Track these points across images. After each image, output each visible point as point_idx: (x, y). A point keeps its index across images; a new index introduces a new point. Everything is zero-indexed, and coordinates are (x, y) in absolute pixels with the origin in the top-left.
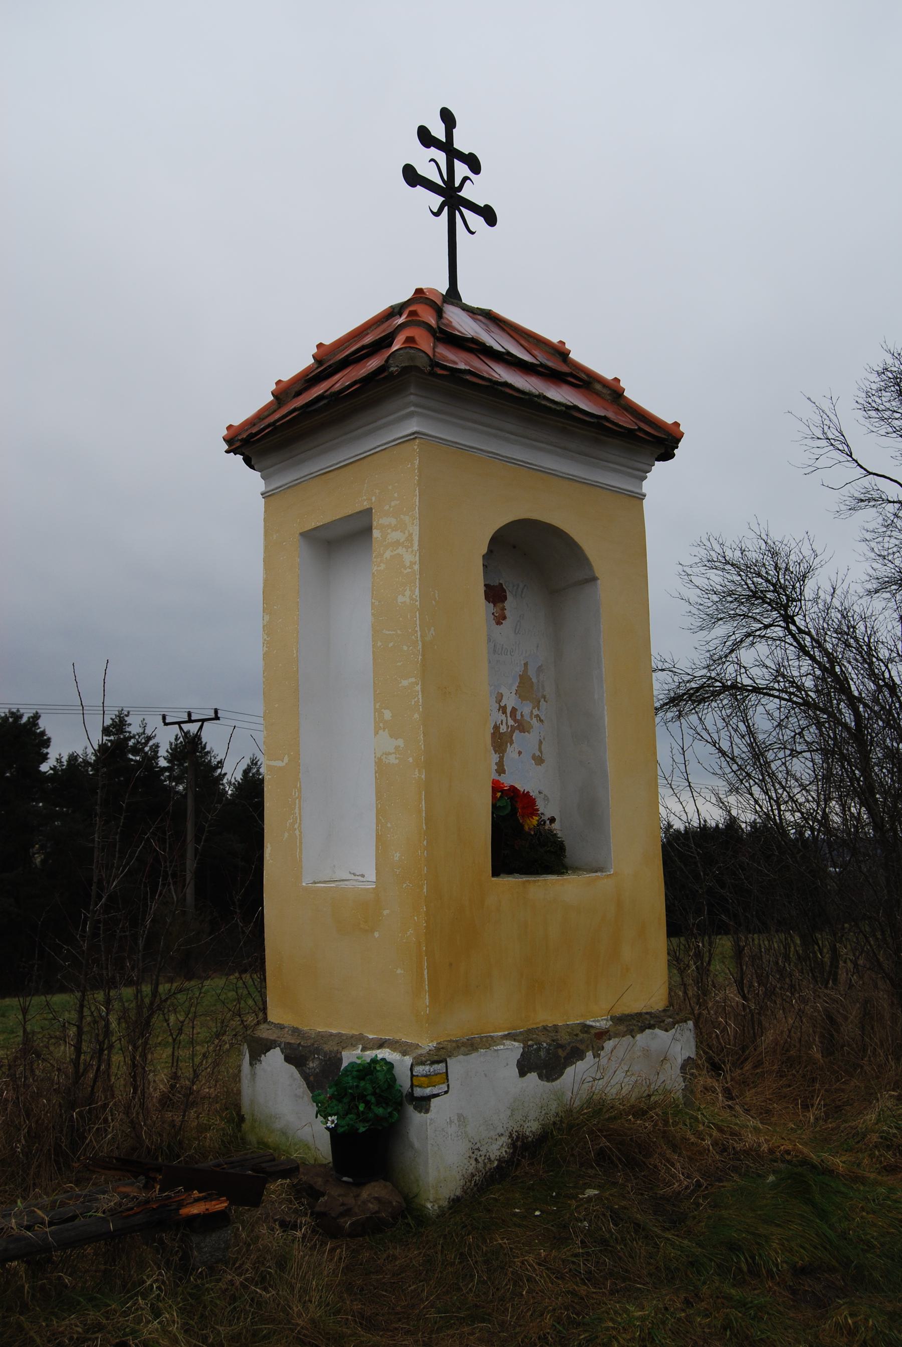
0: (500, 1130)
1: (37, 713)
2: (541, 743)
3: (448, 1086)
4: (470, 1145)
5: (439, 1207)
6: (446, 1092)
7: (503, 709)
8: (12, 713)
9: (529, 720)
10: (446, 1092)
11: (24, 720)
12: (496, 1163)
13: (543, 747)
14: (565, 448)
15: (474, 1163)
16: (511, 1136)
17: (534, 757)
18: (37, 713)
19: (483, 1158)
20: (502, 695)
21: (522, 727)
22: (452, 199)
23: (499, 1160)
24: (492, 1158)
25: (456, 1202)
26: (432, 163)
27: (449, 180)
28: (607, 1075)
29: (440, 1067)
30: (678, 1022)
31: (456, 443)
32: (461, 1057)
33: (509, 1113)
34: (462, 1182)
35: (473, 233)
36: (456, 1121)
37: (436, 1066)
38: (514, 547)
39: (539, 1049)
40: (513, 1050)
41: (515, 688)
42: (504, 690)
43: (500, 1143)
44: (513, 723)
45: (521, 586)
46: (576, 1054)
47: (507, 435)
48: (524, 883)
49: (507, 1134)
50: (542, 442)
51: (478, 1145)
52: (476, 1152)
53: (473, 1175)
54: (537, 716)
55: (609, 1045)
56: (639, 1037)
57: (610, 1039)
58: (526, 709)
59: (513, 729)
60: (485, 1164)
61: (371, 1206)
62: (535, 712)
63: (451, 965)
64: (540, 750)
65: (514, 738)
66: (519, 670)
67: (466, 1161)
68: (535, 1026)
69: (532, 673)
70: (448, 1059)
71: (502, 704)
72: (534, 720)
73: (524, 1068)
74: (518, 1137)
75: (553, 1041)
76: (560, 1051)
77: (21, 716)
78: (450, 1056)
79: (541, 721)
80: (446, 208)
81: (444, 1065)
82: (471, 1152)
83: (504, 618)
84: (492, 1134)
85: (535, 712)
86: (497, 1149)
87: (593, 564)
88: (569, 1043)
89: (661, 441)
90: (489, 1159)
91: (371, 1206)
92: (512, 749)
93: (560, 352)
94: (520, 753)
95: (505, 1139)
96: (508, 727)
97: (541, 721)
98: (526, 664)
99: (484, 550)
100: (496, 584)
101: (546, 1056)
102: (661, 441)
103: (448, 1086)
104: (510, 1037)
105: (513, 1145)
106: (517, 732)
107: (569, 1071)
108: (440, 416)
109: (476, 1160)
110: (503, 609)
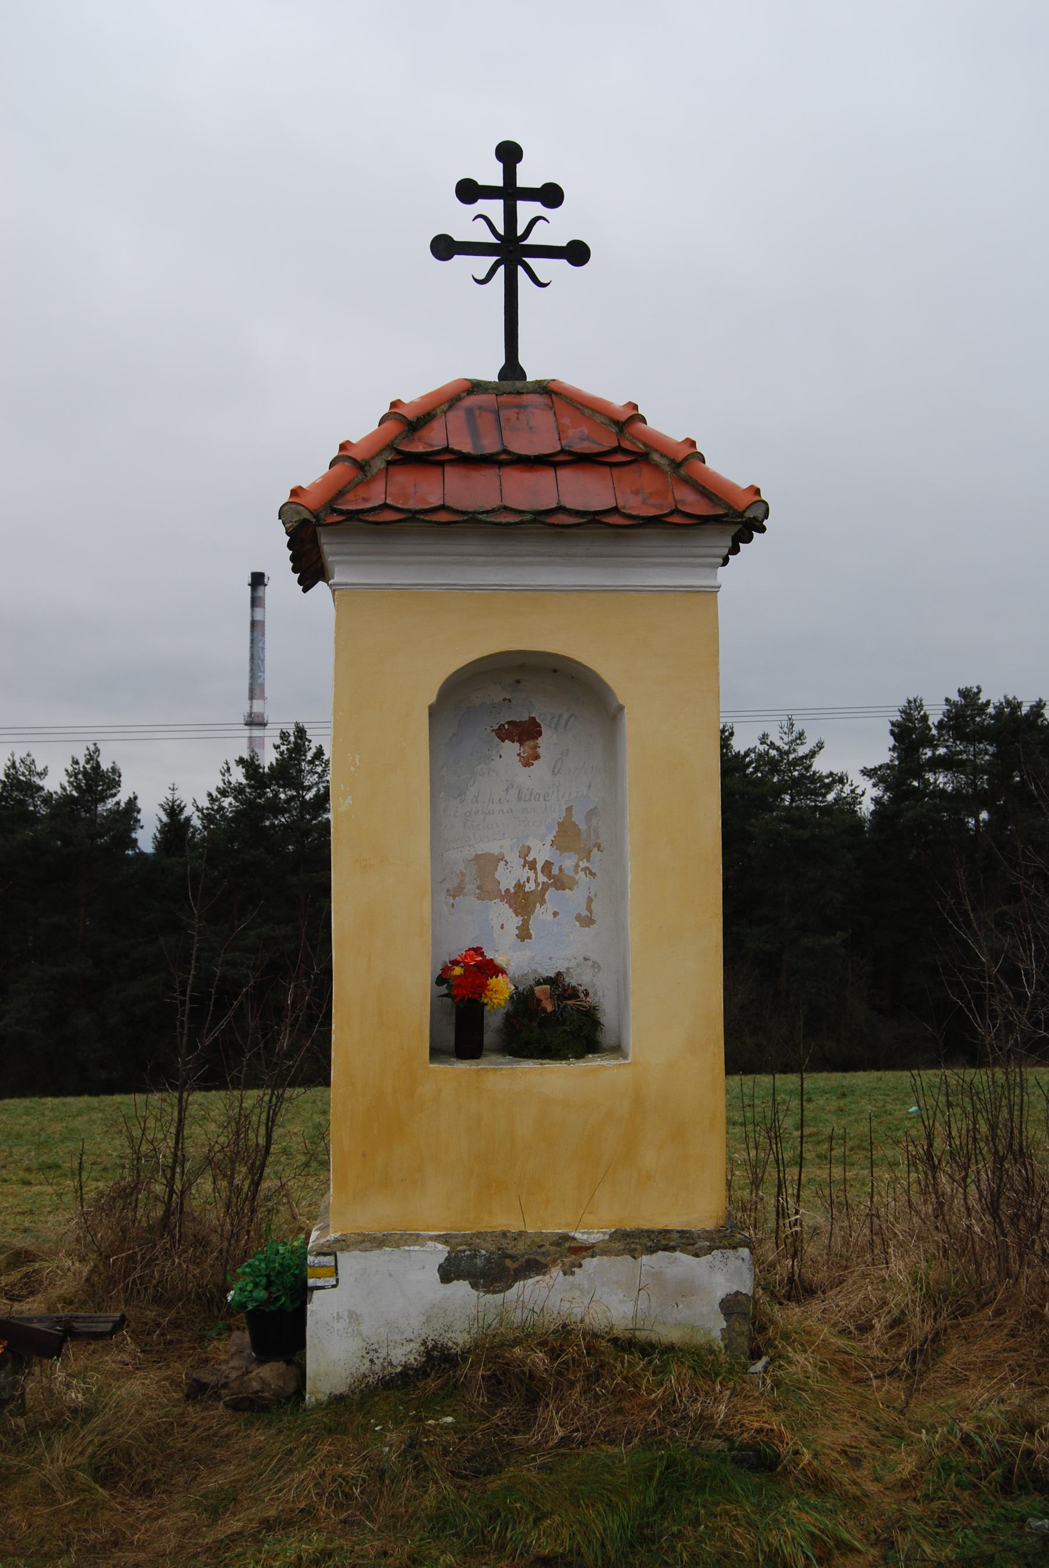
0: (409, 1335)
1: (1041, 700)
2: (590, 900)
3: (337, 1280)
4: (364, 1345)
5: (317, 1400)
6: (334, 1286)
7: (532, 865)
8: (1008, 703)
9: (572, 874)
10: (334, 1286)
11: (1025, 710)
12: (399, 1369)
13: (593, 905)
14: (567, 555)
15: (368, 1364)
16: (424, 1343)
17: (578, 918)
18: (1041, 700)
19: (381, 1360)
20: (529, 849)
21: (560, 882)
22: (511, 252)
23: (405, 1367)
24: (395, 1362)
25: (337, 1400)
26: (481, 221)
27: (510, 229)
28: (602, 1297)
29: (329, 1260)
30: (718, 1248)
31: (390, 584)
32: (357, 1253)
33: (423, 1319)
34: (349, 1380)
35: (544, 285)
36: (346, 1317)
37: (322, 1258)
38: (555, 671)
39: (474, 1256)
40: (440, 1252)
41: (551, 837)
42: (531, 842)
43: (408, 1347)
44: (546, 879)
45: (566, 716)
46: (533, 1267)
47: (471, 558)
48: (478, 1071)
49: (420, 1340)
50: (528, 556)
51: (375, 1346)
52: (372, 1353)
53: (365, 1376)
54: (586, 869)
55: (590, 1264)
56: (645, 1259)
57: (593, 1257)
58: (568, 862)
59: (545, 887)
60: (384, 1368)
61: (254, 1383)
62: (583, 864)
63: (364, 1155)
64: (589, 908)
65: (546, 897)
66: (558, 815)
67: (358, 1360)
68: (489, 1230)
69: (578, 818)
70: (338, 1254)
71: (530, 858)
72: (582, 874)
73: (448, 1273)
74: (435, 1347)
75: (499, 1249)
76: (508, 1262)
77: (1019, 705)
78: (342, 1250)
79: (592, 874)
80: (502, 267)
81: (332, 1258)
82: (364, 1352)
83: (537, 757)
84: (397, 1337)
85: (583, 864)
86: (404, 1354)
87: (614, 689)
88: (523, 1255)
89: (738, 520)
90: (390, 1363)
91: (254, 1383)
92: (542, 910)
93: (629, 420)
94: (555, 914)
95: (416, 1346)
96: (537, 884)
97: (592, 874)
98: (569, 810)
99: (432, 698)
100: (525, 717)
101: (485, 1264)
102: (738, 520)
103: (337, 1280)
104: (445, 1239)
105: (428, 1353)
106: (552, 890)
107: (518, 1286)
108: (368, 558)
109: (371, 1361)
110: (536, 747)
